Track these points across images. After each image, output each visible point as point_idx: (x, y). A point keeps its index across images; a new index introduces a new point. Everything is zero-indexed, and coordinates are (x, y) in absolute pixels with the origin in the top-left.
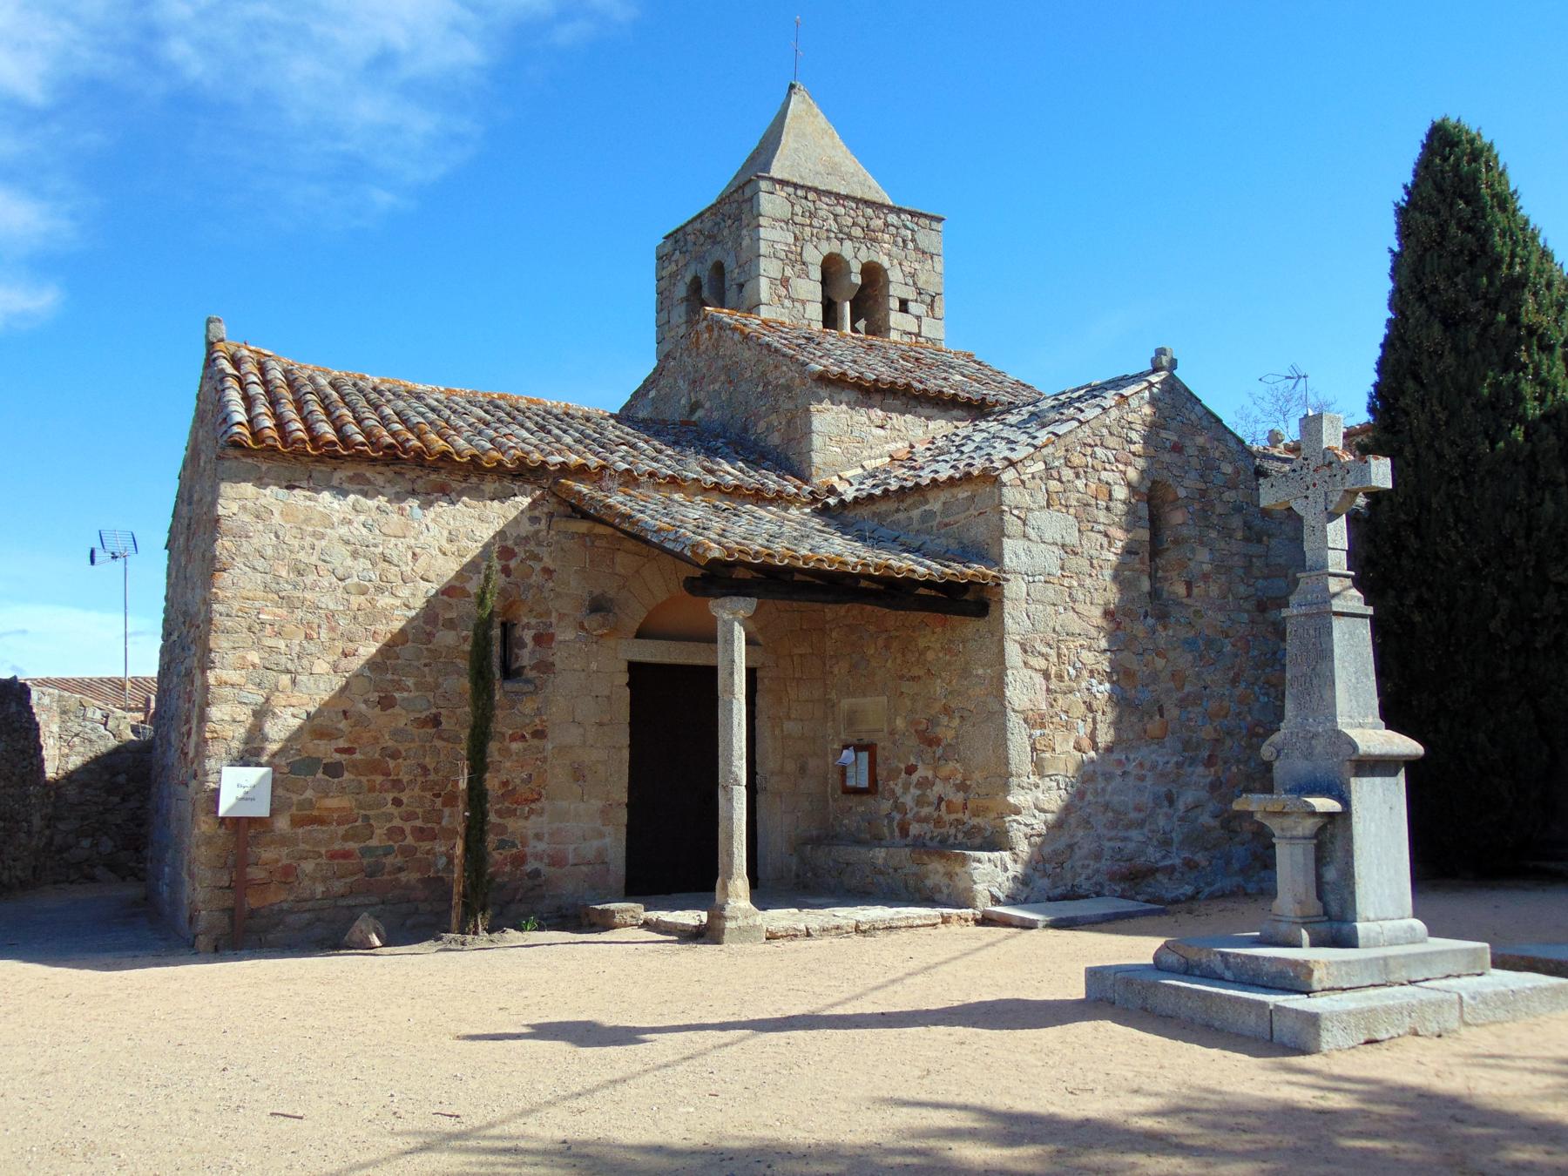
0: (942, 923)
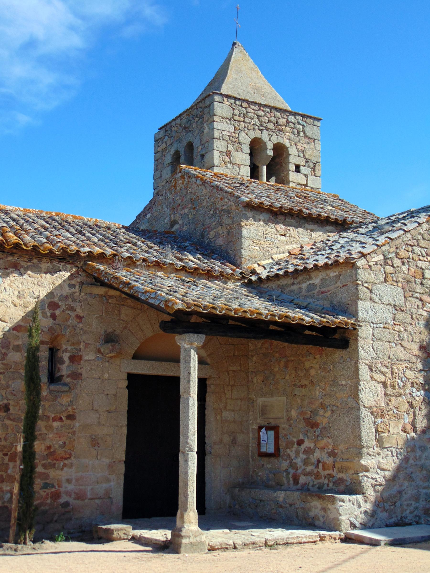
0: (320, 540)
